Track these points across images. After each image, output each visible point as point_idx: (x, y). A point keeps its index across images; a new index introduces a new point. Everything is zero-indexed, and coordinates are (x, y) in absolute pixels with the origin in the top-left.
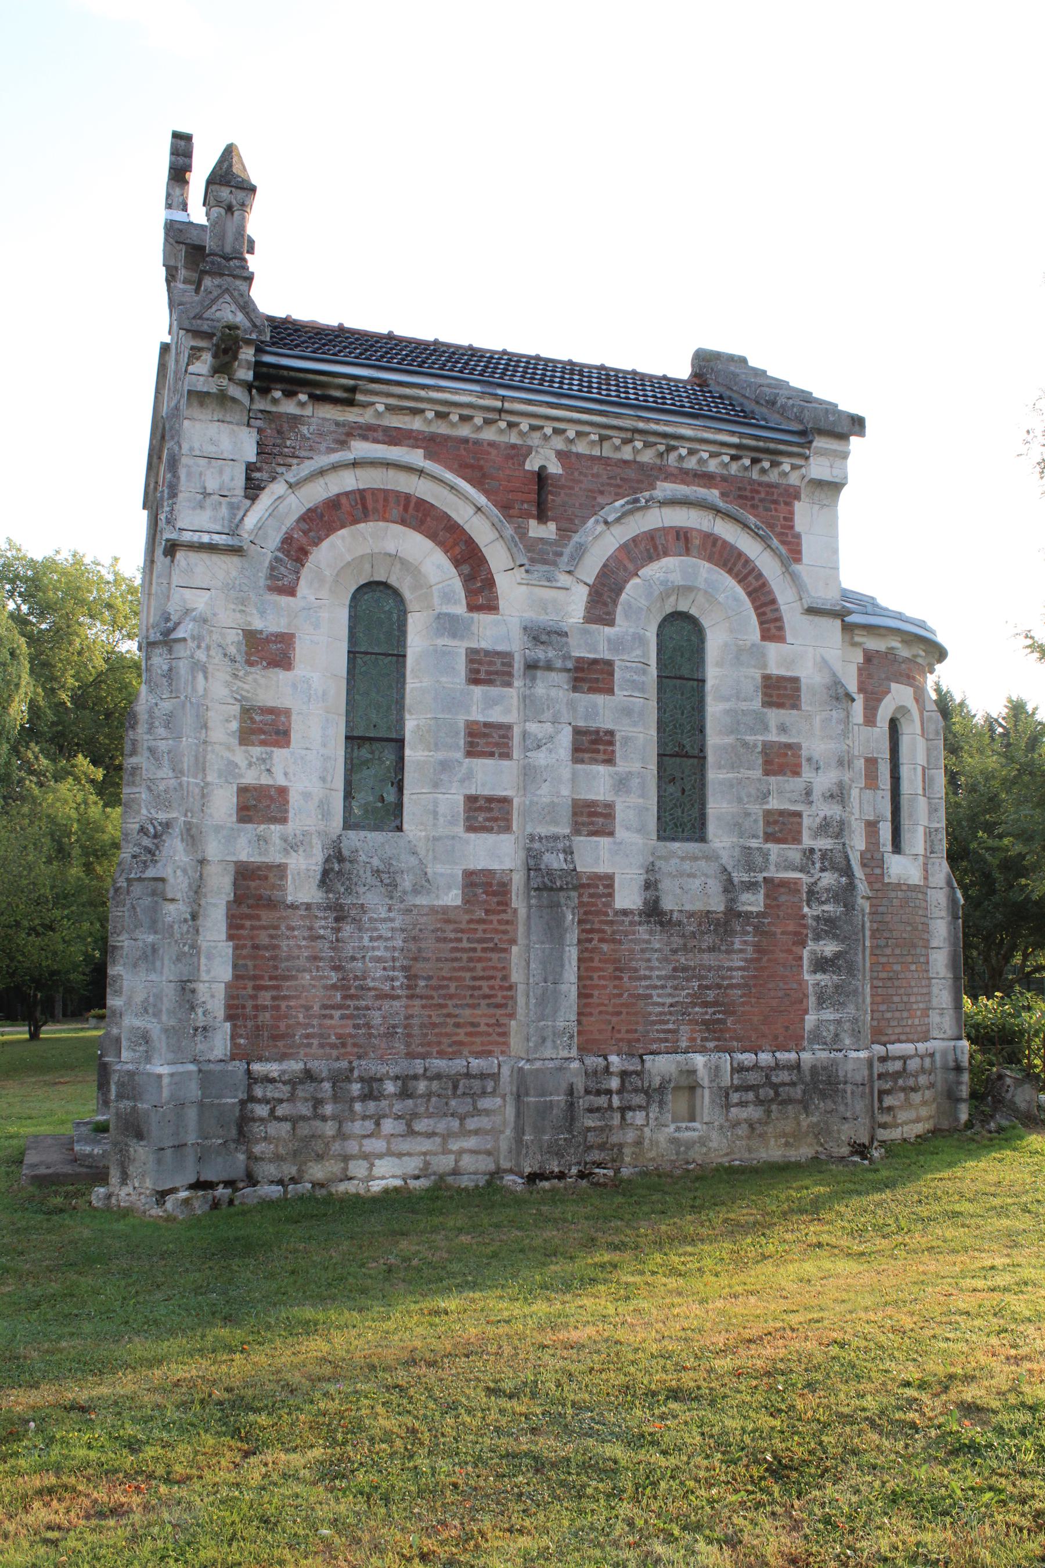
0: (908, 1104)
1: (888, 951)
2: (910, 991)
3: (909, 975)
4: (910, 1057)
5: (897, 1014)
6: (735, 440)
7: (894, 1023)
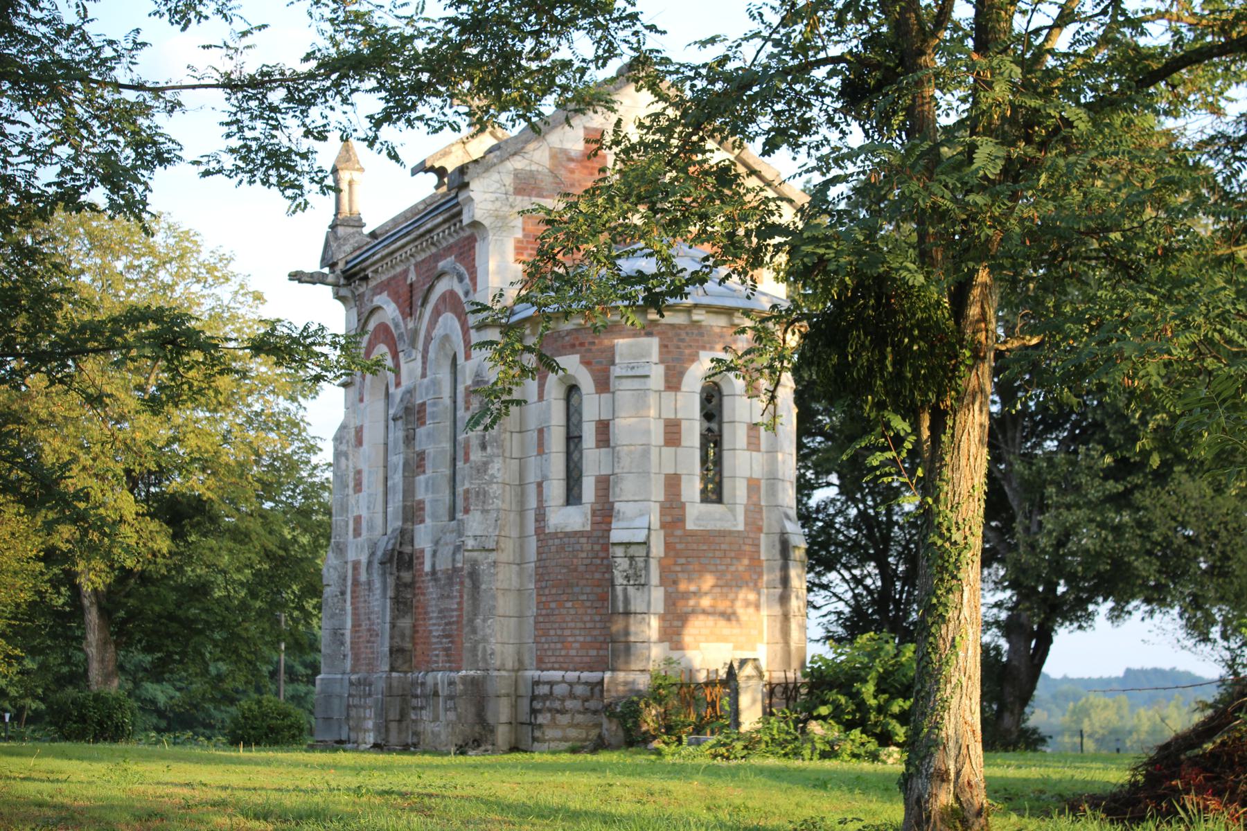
1: (547, 592)
2: (564, 625)
3: (564, 611)
4: (557, 683)
5: (552, 646)
7: (550, 653)
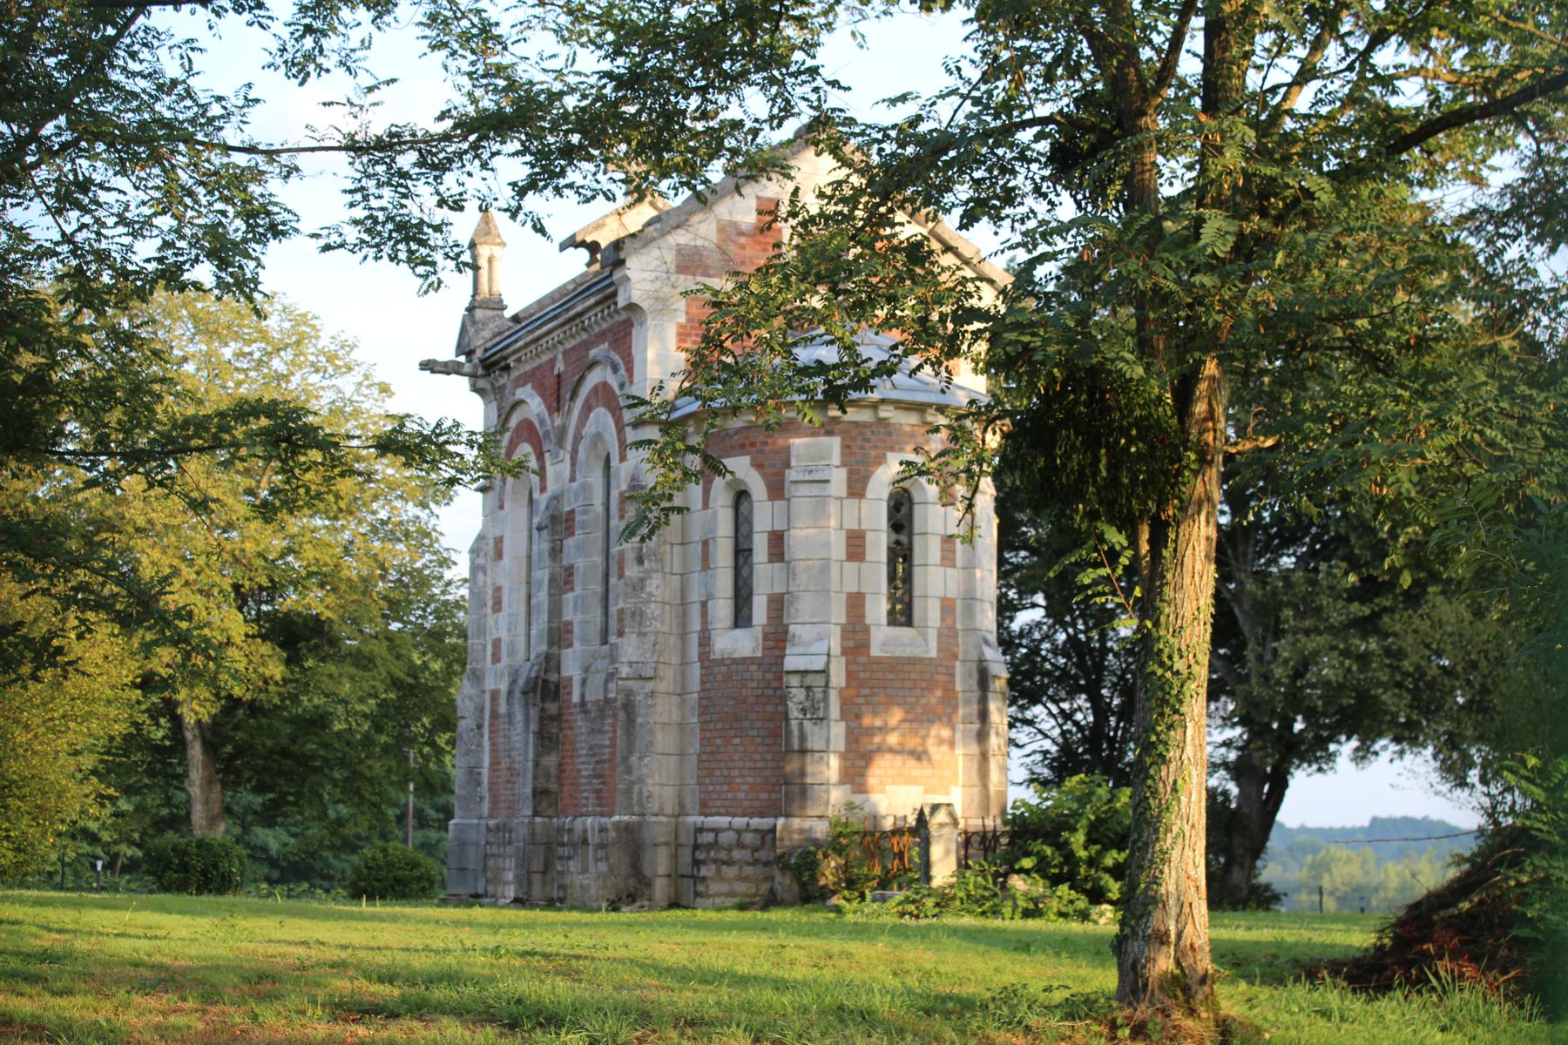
0: (719, 877)
4: (723, 830)
6: (592, 301)
